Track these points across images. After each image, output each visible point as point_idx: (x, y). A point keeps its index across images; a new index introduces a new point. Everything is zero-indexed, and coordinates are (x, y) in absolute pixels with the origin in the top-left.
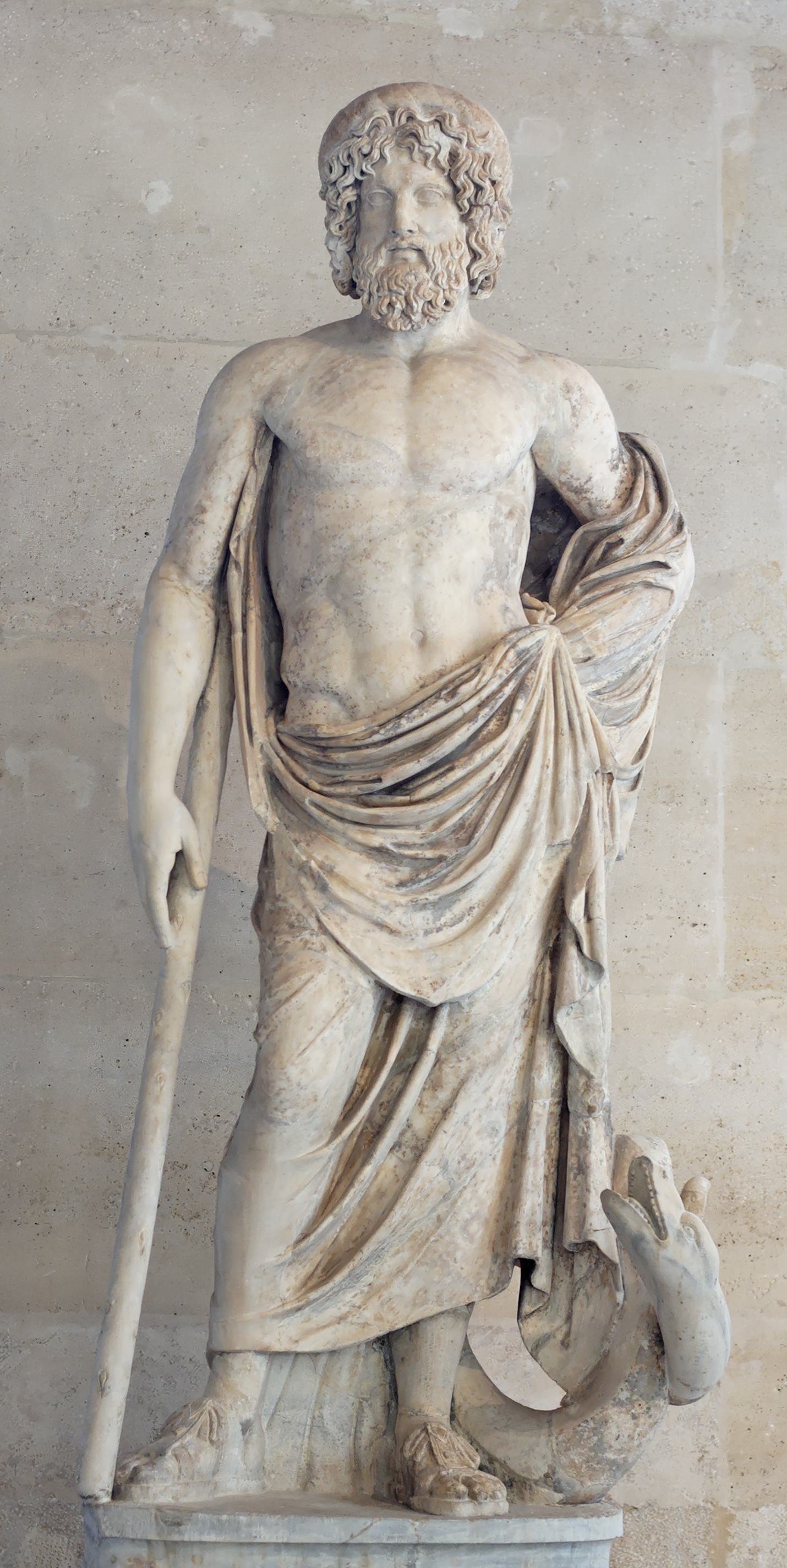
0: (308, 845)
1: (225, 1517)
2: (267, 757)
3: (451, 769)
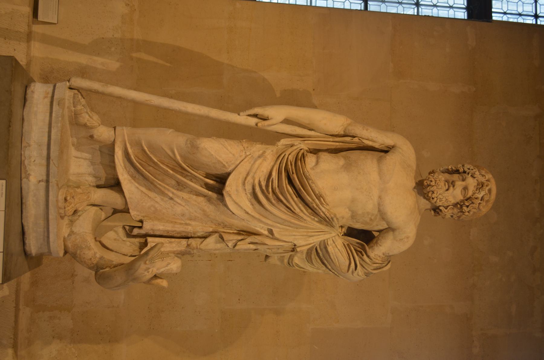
1: (60, 119)
2: (297, 145)
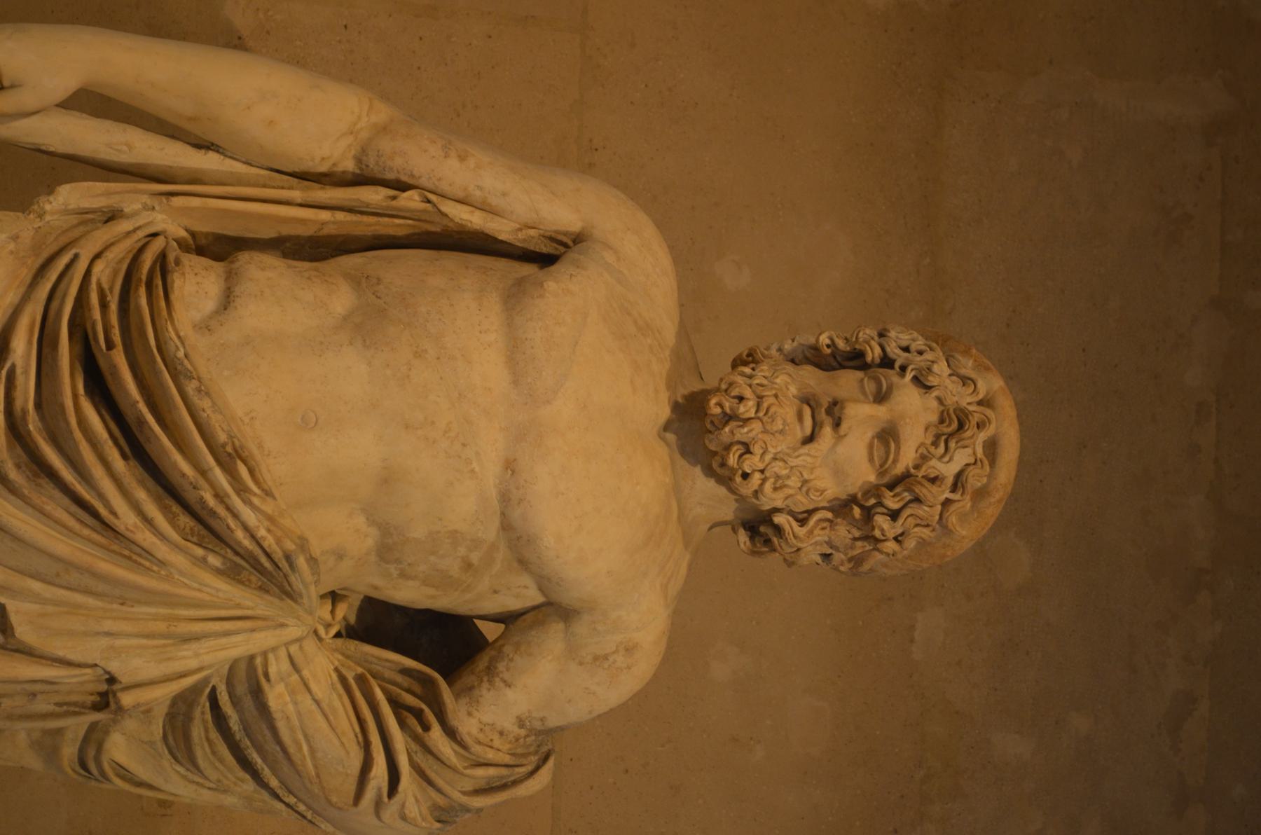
0: (12, 252)
3: (124, 456)
